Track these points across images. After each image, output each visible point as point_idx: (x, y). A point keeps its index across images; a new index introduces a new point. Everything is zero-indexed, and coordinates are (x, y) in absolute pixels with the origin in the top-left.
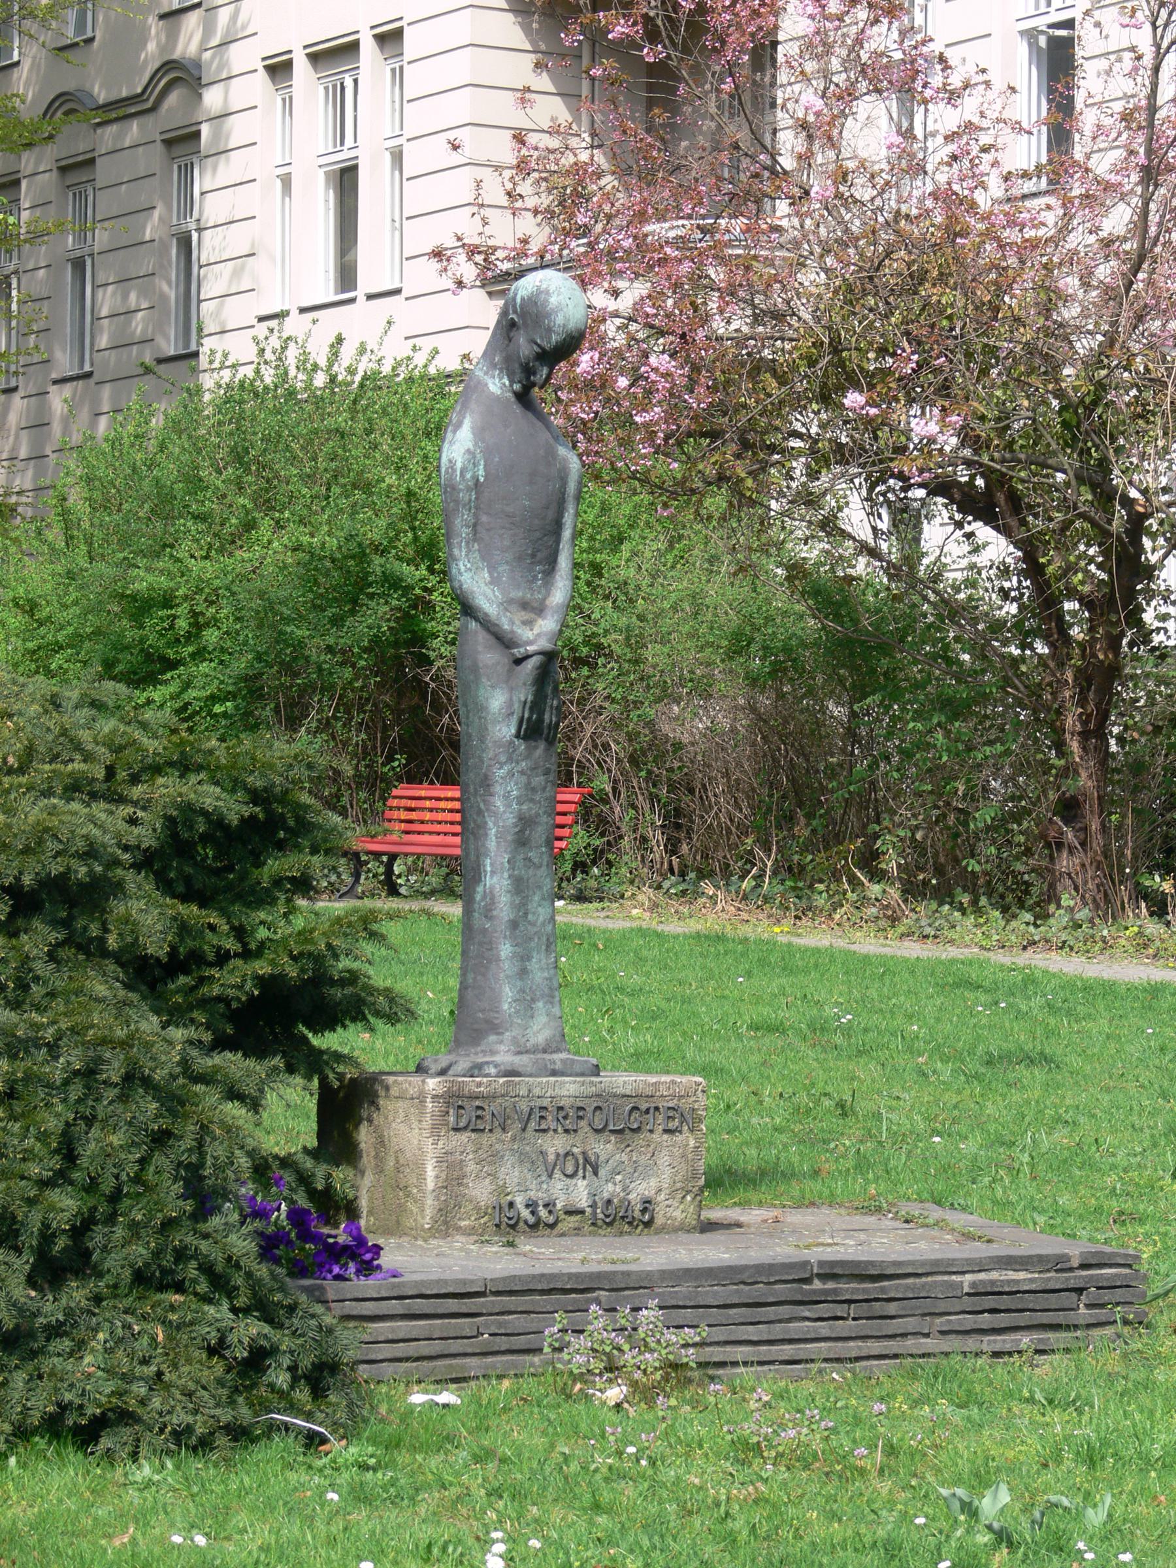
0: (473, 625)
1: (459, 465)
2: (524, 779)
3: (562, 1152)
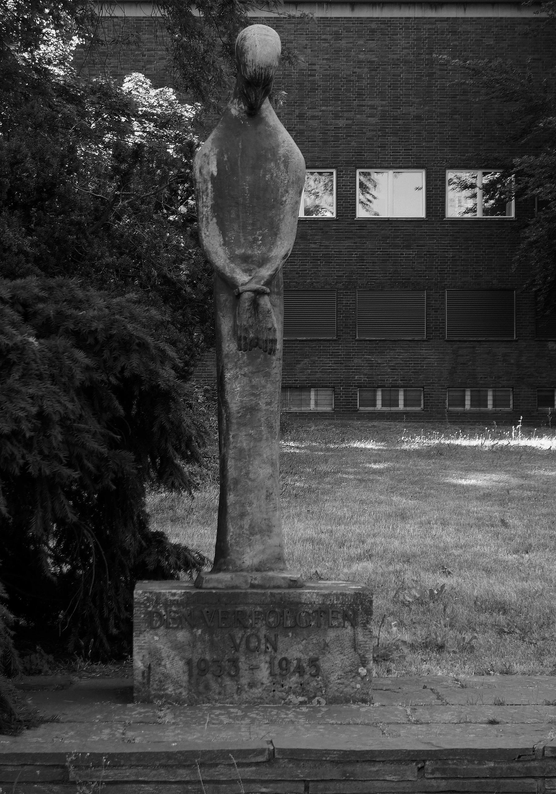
2: (246, 380)
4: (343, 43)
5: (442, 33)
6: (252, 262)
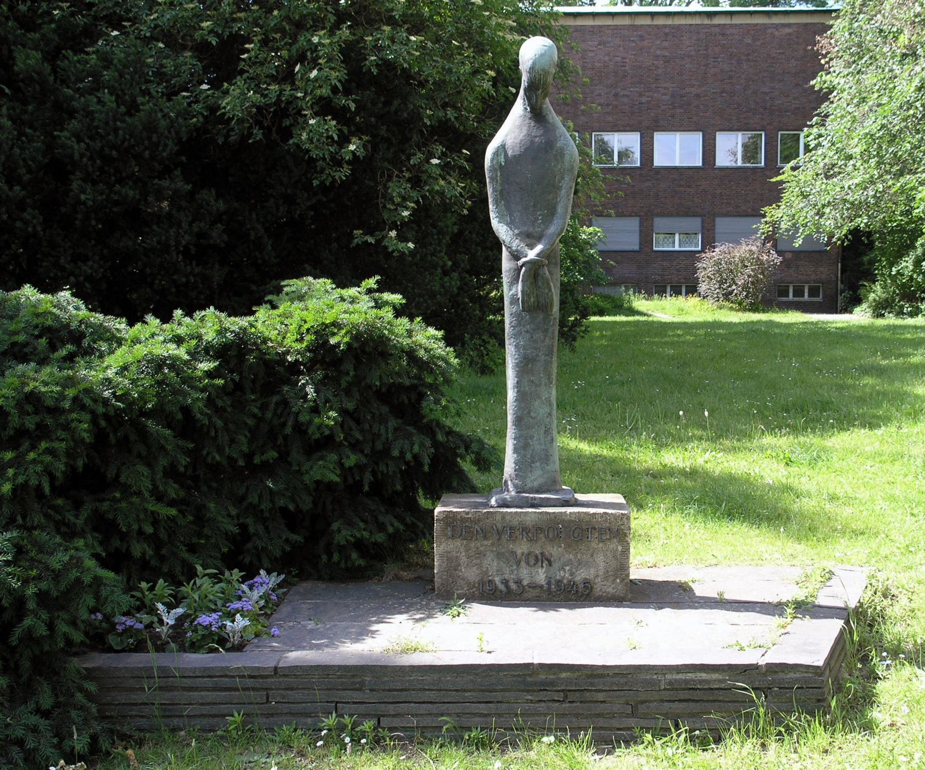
2: (528, 336)
3: (526, 552)
4: (645, 43)
5: (715, 35)
6: (534, 237)
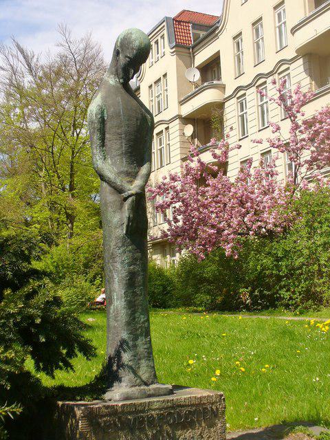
0: (105, 184)
1: (94, 112)
